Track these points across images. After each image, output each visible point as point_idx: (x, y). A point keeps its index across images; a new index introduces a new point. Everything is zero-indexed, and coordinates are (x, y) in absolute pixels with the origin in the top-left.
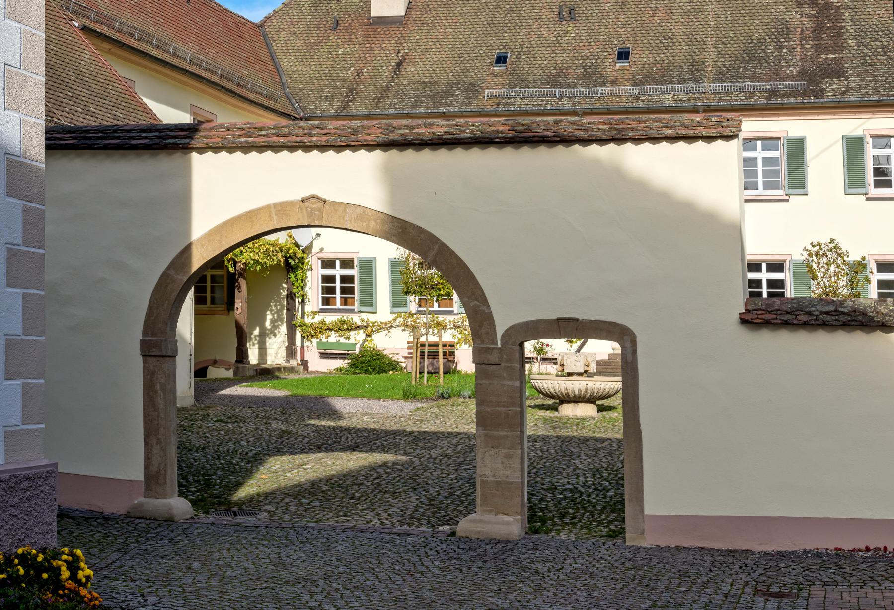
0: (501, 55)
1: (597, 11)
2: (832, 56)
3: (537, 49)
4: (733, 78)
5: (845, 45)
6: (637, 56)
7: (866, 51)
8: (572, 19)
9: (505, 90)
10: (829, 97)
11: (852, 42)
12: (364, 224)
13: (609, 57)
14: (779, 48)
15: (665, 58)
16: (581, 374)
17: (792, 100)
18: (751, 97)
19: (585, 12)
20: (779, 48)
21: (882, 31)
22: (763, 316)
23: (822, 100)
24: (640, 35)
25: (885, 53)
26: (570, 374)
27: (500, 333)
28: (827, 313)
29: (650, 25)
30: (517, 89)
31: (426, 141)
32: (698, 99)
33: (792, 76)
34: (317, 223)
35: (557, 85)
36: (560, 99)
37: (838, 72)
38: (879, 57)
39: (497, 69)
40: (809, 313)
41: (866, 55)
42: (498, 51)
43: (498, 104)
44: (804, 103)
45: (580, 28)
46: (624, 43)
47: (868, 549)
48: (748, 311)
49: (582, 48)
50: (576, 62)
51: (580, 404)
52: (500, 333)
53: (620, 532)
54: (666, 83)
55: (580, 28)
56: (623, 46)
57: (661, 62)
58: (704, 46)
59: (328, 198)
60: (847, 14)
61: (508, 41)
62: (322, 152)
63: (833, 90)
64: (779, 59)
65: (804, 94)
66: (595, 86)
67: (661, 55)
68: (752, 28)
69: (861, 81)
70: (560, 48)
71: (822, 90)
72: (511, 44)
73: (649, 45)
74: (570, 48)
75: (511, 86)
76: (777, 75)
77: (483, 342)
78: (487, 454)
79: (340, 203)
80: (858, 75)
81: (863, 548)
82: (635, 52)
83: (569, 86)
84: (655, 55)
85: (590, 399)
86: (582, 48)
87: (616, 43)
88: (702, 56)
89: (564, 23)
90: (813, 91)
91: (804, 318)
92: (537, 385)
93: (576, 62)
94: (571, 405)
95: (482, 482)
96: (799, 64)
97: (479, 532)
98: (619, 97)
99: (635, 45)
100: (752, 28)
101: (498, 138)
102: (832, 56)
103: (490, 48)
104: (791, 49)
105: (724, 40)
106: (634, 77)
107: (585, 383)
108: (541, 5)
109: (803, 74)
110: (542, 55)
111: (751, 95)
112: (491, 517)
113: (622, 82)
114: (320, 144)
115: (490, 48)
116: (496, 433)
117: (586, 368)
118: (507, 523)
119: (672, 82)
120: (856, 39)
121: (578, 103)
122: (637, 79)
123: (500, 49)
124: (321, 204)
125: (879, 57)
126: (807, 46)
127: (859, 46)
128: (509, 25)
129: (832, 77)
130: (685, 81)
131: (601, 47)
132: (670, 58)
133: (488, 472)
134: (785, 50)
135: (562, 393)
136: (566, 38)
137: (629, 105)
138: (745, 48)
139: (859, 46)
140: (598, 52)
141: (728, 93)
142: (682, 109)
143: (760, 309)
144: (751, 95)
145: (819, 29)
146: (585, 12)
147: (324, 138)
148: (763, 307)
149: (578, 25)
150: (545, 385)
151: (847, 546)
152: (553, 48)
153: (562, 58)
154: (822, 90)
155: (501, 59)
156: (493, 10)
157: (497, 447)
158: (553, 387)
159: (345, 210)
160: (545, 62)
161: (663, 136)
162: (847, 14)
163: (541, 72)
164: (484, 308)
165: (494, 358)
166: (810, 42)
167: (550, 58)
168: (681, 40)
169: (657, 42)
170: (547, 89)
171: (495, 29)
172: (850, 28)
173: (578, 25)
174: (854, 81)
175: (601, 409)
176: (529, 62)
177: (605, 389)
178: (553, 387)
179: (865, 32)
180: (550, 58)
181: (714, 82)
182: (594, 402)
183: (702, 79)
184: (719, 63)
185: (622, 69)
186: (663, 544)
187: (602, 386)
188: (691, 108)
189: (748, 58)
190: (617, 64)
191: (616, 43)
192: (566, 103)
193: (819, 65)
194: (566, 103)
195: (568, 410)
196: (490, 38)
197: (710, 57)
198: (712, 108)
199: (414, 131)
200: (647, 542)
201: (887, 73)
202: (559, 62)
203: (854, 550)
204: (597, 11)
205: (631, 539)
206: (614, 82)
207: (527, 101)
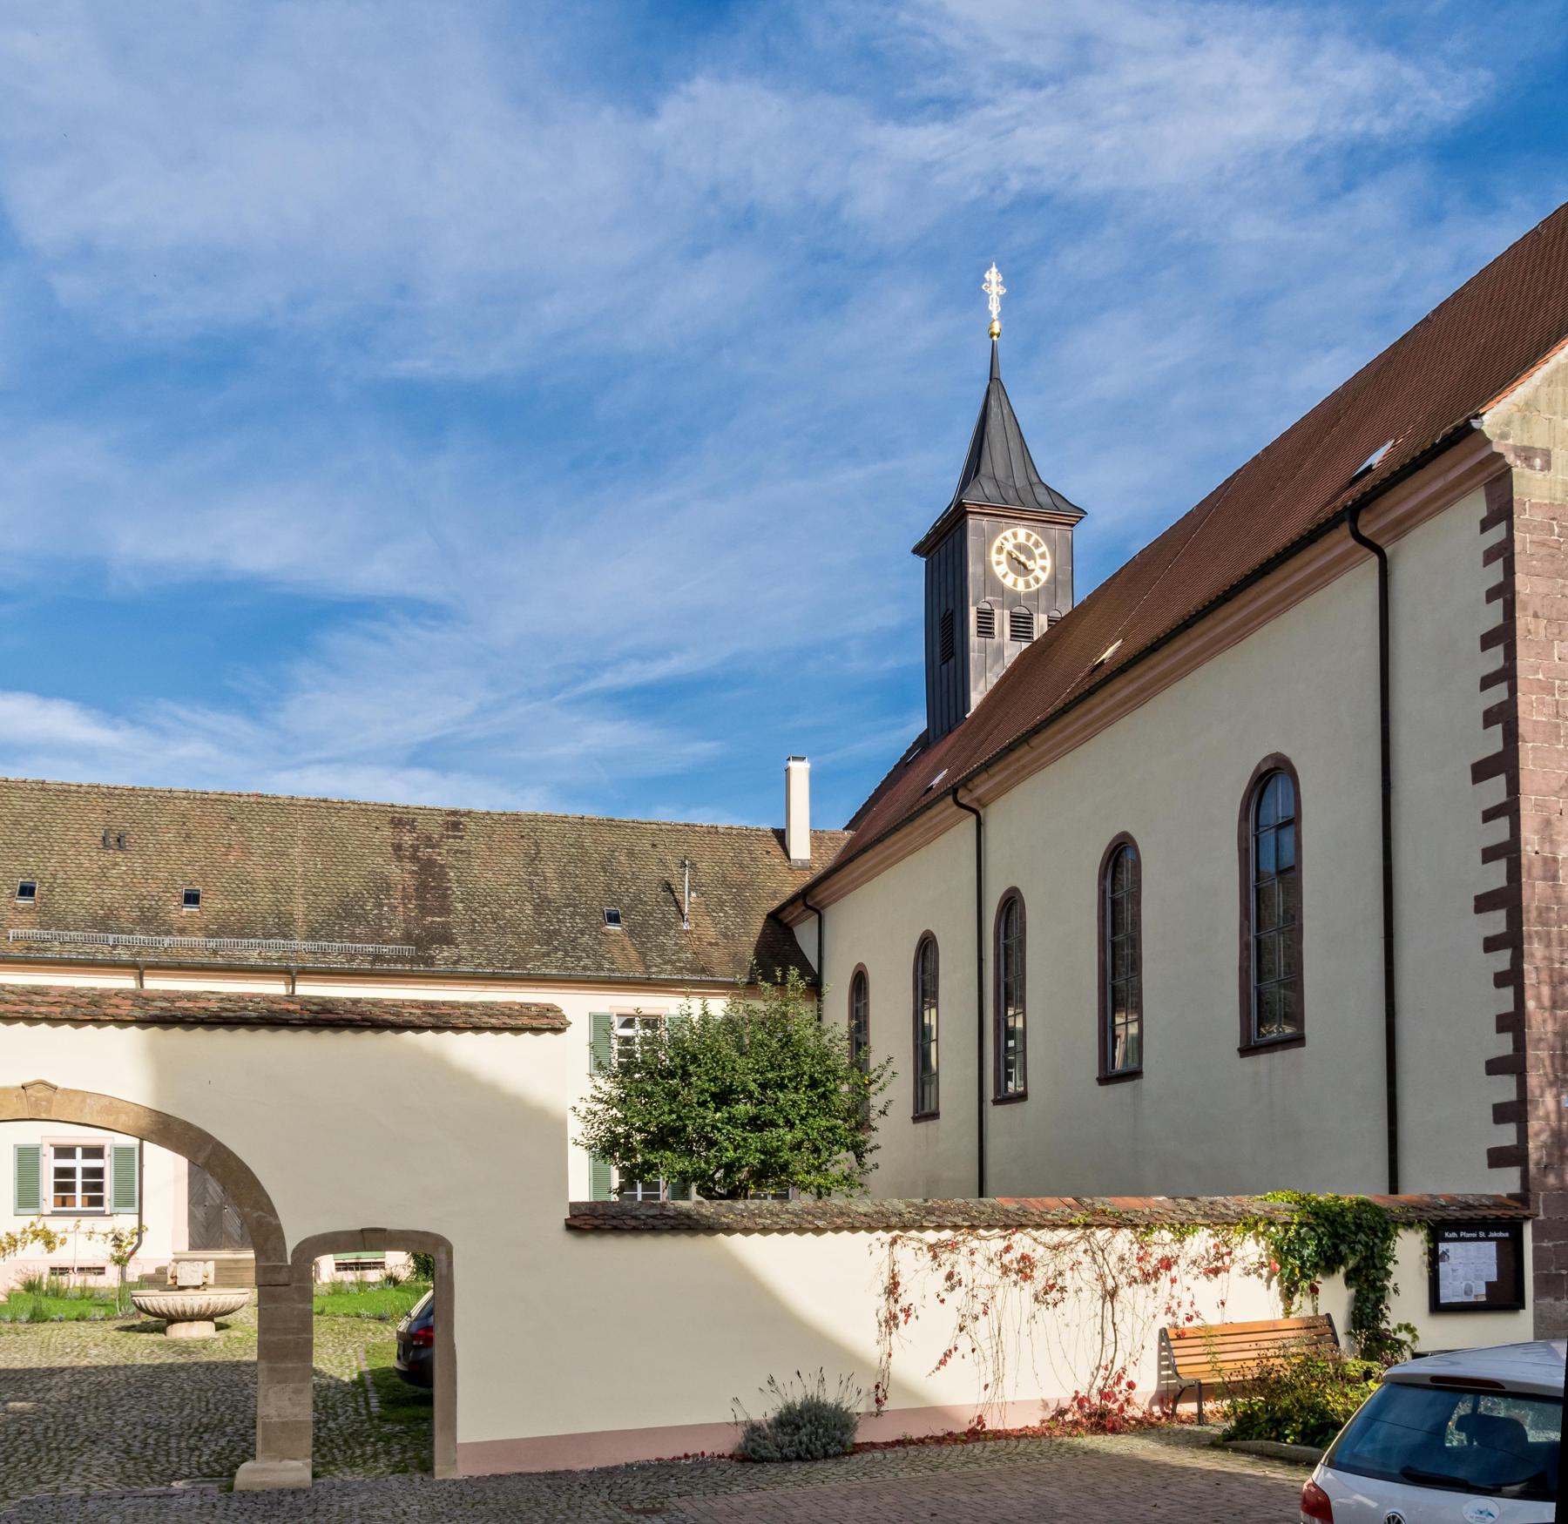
0: (26, 885)
1: (154, 842)
2: (439, 919)
3: (76, 881)
4: (330, 937)
5: (452, 908)
6: (209, 901)
7: (474, 916)
8: (121, 848)
9: (35, 931)
10: (441, 967)
11: (460, 906)
12: (112, 1118)
13: (173, 899)
14: (380, 906)
15: (244, 906)
16: (197, 1287)
17: (399, 967)
18: (353, 960)
19: (139, 841)
20: (380, 906)
21: (490, 896)
22: (591, 1222)
23: (433, 969)
24: (211, 876)
25: (495, 921)
26: (182, 1288)
27: (290, 1246)
28: (653, 1217)
29: (223, 865)
30: (53, 931)
31: (203, 1019)
32: (288, 958)
33: (396, 939)
34: (44, 1116)
35: (107, 929)
36: (114, 947)
37: (447, 939)
38: (489, 925)
39: (23, 902)
40: (635, 1217)
41: (475, 921)
42: (21, 880)
43: (29, 948)
44: (413, 971)
45: (133, 860)
46: (191, 884)
47: (686, 1456)
48: (574, 1217)
49: (138, 885)
50: (129, 902)
51: (196, 1322)
52: (290, 1246)
53: (427, 1467)
54: (248, 936)
55: (133, 860)
56: (190, 887)
57: (239, 910)
58: (292, 896)
59: (60, 1085)
60: (452, 874)
61: (35, 868)
62: (8, 1024)
63: (444, 957)
64: (380, 917)
65: (412, 961)
66: (158, 934)
67: (239, 902)
68: (347, 879)
69: (474, 950)
70: (107, 883)
71: (433, 957)
72: (38, 872)
73: (223, 889)
74: (121, 884)
75: (44, 926)
76: (377, 936)
77: (268, 1260)
78: (271, 1392)
79: (76, 1092)
80: (469, 943)
81: (682, 1455)
82: (206, 896)
83: (123, 932)
84: (232, 902)
85: (209, 1317)
86: (138, 885)
87: (181, 883)
88: (289, 908)
89: (111, 851)
90: (422, 957)
91: (633, 1223)
92: (142, 1303)
93: (129, 902)
94: (186, 1324)
95: (265, 1424)
96: (403, 925)
97: (264, 1483)
98: (192, 949)
99: (207, 888)
100: (347, 879)
101: (296, 1019)
102: (439, 919)
103: (9, 874)
104: (393, 908)
105: (314, 890)
106: (207, 926)
107: (207, 1297)
108: (77, 826)
109: (408, 938)
110: (83, 890)
111: (352, 958)
112: (274, 1464)
113: (192, 932)
114: (53, 1016)
115: (9, 874)
116: (283, 1366)
117: (205, 1280)
118: (298, 1469)
119: (255, 936)
120: (462, 902)
121: (139, 954)
122: (211, 929)
123: (24, 878)
124: (49, 1093)
125: (489, 925)
126: (410, 906)
127: (467, 911)
128: (35, 847)
129: (441, 944)
130: (271, 936)
131: (163, 886)
132: (251, 907)
133: (272, 1412)
134: (385, 909)
135: (176, 1311)
136: (115, 871)
137: (205, 960)
138: (339, 903)
139: (467, 911)
140: (158, 892)
141: (325, 954)
142: (272, 969)
143: (586, 1215)
144: (352, 958)
145: (422, 888)
146: (139, 841)
147: (58, 1010)
148: (588, 1212)
149: (129, 856)
150: (155, 1304)
151: (667, 1455)
152: (98, 883)
153: (110, 896)
154: (433, 957)
155: (27, 891)
156: (11, 826)
157: (285, 1382)
158: (166, 1305)
159: (84, 1101)
160: (88, 899)
161: (489, 1025)
162: (452, 874)
163: (83, 911)
164: (271, 1219)
165: (282, 1277)
166: (414, 902)
167: (94, 895)
168: (262, 886)
169: (234, 886)
170: (94, 934)
171: (14, 850)
172: (457, 890)
173: (129, 856)
174: (465, 950)
175: (219, 1327)
176: (66, 898)
177: (231, 1303)
178: (166, 1305)
179: (472, 896)
180: (94, 895)
181: (306, 939)
182: (212, 1320)
183: (292, 935)
184: (311, 917)
185: (192, 915)
186: (476, 1474)
187: (228, 1301)
188: (283, 969)
189: (344, 915)
190: (185, 909)
191: (181, 883)
192: (122, 952)
193: (424, 928)
194: (122, 952)
195: (179, 1331)
196: (9, 862)
197: (299, 909)
198: (307, 970)
199: (177, 1004)
200: (460, 1473)
201: (499, 943)
202: (107, 900)
203: (674, 1458)
204: (154, 842)
205: (441, 1472)
206: (182, 931)
207: (68, 947)
